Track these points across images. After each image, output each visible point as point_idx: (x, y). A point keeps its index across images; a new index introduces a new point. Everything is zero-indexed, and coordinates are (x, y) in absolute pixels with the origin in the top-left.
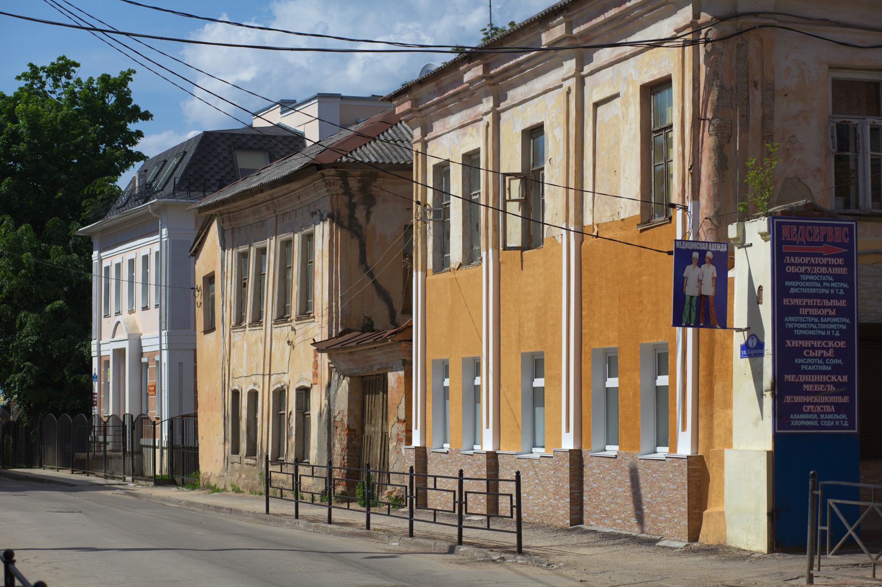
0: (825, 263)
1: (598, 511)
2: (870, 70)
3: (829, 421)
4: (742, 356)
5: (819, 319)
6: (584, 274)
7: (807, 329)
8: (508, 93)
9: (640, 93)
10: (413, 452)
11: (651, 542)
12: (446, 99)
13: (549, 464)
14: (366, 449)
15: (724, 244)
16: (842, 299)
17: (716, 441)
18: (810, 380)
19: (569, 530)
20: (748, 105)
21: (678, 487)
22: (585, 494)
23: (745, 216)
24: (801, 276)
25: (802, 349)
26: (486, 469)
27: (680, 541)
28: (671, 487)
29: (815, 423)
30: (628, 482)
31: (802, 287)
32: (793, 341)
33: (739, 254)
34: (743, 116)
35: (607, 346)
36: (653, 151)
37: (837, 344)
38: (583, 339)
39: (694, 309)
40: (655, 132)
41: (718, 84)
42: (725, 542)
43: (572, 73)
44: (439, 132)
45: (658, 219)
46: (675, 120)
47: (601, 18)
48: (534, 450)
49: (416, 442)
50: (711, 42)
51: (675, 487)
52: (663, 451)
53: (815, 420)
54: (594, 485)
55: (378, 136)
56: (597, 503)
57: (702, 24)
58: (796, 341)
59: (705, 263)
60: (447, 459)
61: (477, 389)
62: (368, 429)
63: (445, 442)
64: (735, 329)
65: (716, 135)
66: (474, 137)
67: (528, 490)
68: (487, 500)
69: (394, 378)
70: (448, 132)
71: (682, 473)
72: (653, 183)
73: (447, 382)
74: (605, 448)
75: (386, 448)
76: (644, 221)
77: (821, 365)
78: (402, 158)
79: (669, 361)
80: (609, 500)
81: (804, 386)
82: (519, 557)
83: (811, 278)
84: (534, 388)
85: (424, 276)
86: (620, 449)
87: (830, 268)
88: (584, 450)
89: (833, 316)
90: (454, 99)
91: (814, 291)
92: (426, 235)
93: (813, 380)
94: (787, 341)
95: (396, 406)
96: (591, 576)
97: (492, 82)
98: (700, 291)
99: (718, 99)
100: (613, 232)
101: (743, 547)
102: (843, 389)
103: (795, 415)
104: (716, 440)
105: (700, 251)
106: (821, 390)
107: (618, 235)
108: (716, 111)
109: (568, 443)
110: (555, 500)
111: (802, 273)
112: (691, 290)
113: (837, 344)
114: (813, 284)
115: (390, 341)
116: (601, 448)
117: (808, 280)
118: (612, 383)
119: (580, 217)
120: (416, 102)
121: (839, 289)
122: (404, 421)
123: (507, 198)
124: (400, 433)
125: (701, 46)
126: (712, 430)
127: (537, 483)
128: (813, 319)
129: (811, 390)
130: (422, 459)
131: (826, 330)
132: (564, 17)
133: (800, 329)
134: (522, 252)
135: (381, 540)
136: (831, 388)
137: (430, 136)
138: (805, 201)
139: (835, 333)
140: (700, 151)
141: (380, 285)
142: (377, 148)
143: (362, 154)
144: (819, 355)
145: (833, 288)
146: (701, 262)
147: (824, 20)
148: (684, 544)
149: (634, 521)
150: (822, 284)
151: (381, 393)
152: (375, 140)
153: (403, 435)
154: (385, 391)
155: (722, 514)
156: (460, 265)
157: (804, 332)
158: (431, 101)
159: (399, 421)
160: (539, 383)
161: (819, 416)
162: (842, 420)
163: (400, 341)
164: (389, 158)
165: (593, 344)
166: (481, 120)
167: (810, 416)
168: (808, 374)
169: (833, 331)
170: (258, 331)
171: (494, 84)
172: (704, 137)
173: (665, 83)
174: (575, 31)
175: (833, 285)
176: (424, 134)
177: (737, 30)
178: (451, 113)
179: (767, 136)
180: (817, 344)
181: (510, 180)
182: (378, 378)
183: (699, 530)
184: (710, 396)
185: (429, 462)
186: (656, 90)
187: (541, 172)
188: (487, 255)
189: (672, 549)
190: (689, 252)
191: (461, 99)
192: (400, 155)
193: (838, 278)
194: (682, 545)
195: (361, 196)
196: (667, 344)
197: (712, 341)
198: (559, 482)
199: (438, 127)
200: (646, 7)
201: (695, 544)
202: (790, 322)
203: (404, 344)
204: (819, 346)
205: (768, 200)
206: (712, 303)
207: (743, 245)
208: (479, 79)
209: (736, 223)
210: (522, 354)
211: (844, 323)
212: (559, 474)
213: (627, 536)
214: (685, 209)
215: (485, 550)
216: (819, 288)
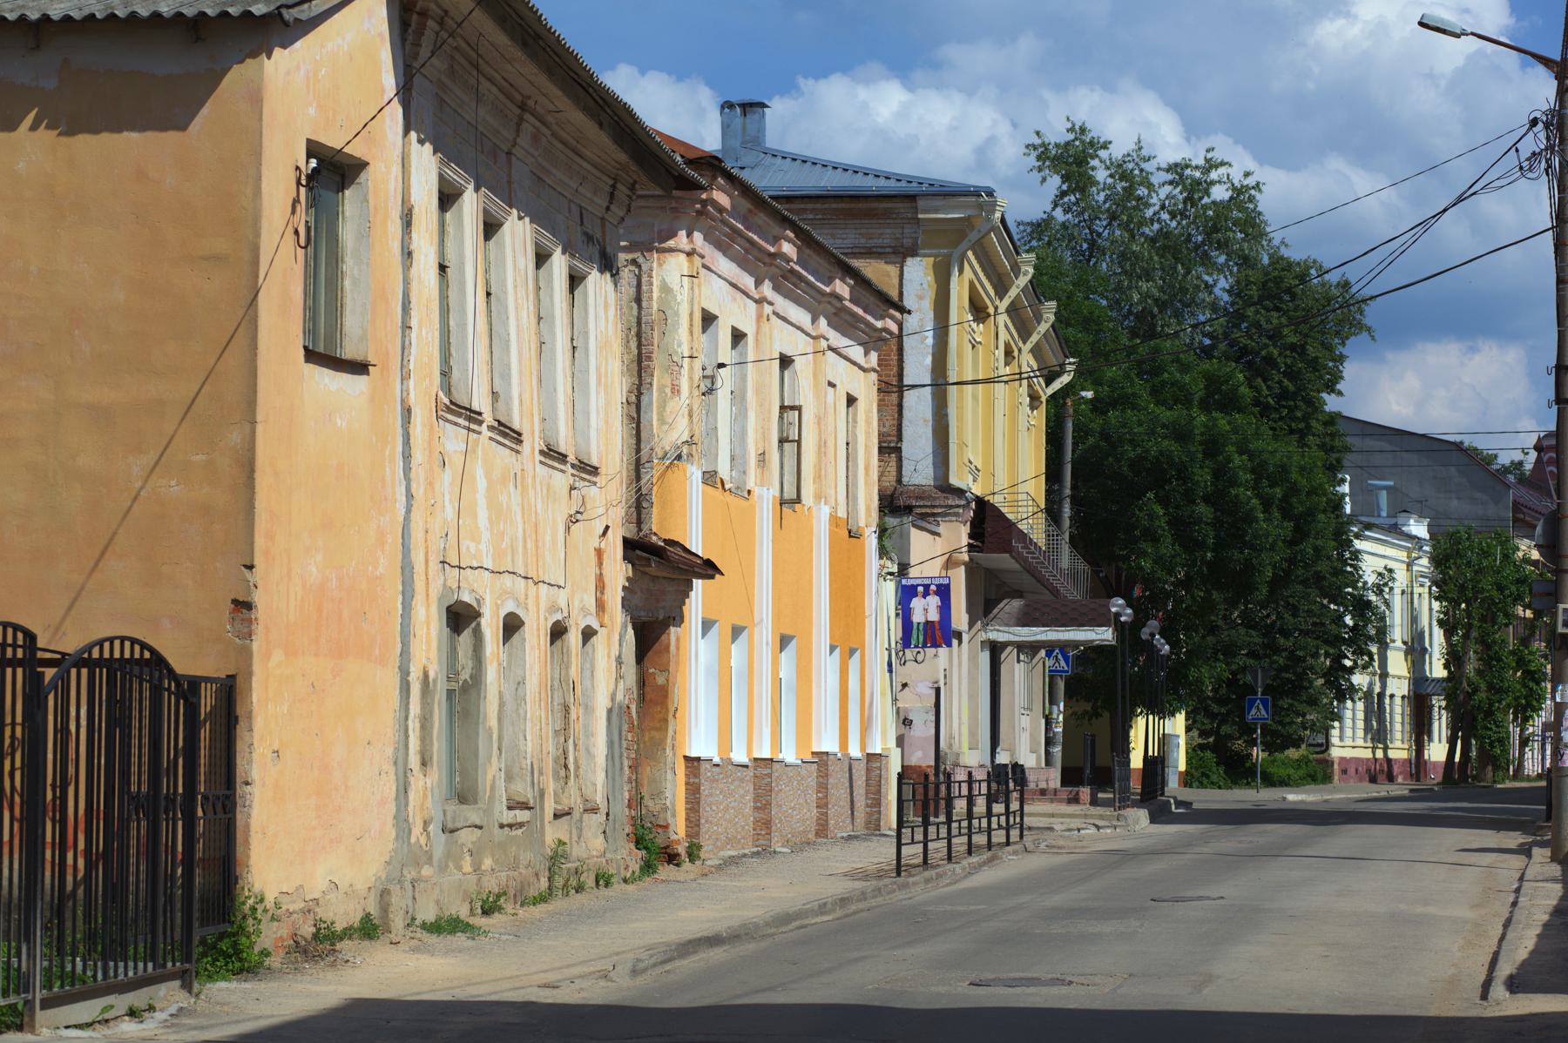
39: (921, 633)
105: (924, 586)
112: (918, 618)
146: (926, 594)
170: (507, 451)
206: (937, 627)
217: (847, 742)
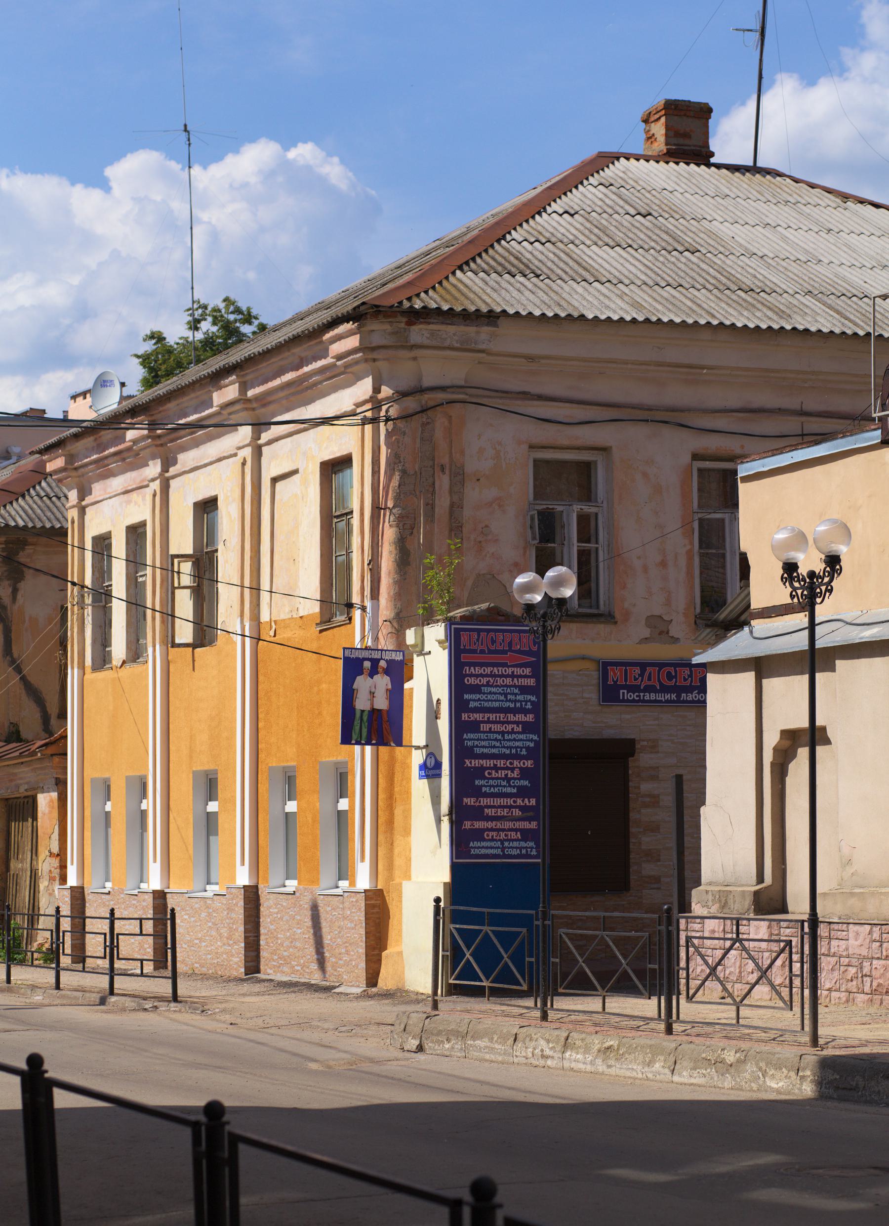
0: (510, 673)
1: (276, 957)
2: (578, 448)
3: (515, 850)
4: (421, 777)
5: (503, 736)
6: (261, 678)
7: (488, 747)
8: (178, 456)
9: (321, 471)
10: (67, 893)
11: (328, 989)
12: (106, 457)
13: (222, 904)
14: (12, 891)
15: (400, 651)
16: (529, 713)
17: (397, 873)
18: (492, 804)
19: (242, 980)
20: (433, 493)
21: (356, 925)
22: (262, 937)
23: (428, 619)
24: (483, 688)
25: (483, 769)
26: (152, 912)
27: (358, 986)
28: (349, 925)
29: (499, 852)
30: (308, 923)
31: (484, 700)
32: (473, 761)
33: (418, 661)
34: (427, 504)
35: (286, 764)
36: (334, 539)
37: (524, 764)
38: (260, 756)
40: (337, 517)
41: (400, 468)
42: (404, 986)
43: (248, 441)
44: (100, 496)
45: (340, 618)
46: (355, 506)
47: (277, 382)
48: (208, 887)
49: (72, 880)
50: (392, 420)
51: (353, 925)
52: (344, 884)
53: (498, 848)
54: (272, 927)
55: (28, 491)
56: (274, 948)
57: (383, 400)
58: (477, 761)
59: (377, 673)
60: (109, 901)
61: (144, 813)
62: (13, 864)
63: (107, 880)
64: (414, 746)
65: (398, 526)
66: (139, 506)
67: (200, 935)
68: (154, 949)
69: (45, 801)
70: (110, 498)
71: (360, 909)
72: (334, 576)
73: (108, 807)
74: (284, 883)
75: (37, 889)
76: (324, 620)
77: (504, 786)
78: (58, 520)
79: (349, 782)
80: (286, 943)
81: (486, 810)
82: (173, 1004)
83: (494, 690)
84: (208, 813)
85: (82, 673)
86: (299, 884)
87: (515, 679)
88: (261, 886)
89: (519, 733)
90: (115, 458)
91: (496, 704)
92: (84, 623)
93: (495, 804)
94: (467, 761)
95: (47, 837)
96: (245, 1021)
97: (159, 442)
98: (372, 704)
99: (399, 485)
100: (292, 631)
101: (421, 991)
102: (531, 814)
103: (475, 842)
104: (397, 872)
106: (505, 814)
107: (296, 635)
108: (397, 499)
109: (243, 878)
110: (229, 945)
111: (483, 685)
112: (362, 703)
113: (524, 764)
114: (495, 697)
115: (39, 755)
116: (280, 883)
117: (490, 693)
118: (291, 807)
119: (256, 612)
120: (71, 458)
121: (526, 702)
122: (58, 855)
123: (176, 585)
124: (53, 869)
125: (382, 424)
126: (392, 861)
127: (210, 927)
128: (496, 736)
129: (493, 814)
130: (79, 902)
131: (511, 748)
132: (237, 376)
133: (481, 747)
134: (193, 649)
135: (23, 995)
136: (517, 813)
137: (88, 500)
138: (488, 604)
139: (521, 751)
140: (380, 544)
141: (30, 682)
142: (27, 507)
143: (7, 515)
144: (503, 776)
145: (519, 701)
146: (373, 672)
147: (524, 393)
148: (362, 989)
149: (314, 966)
150: (506, 697)
151: (30, 820)
152: (23, 496)
153: (56, 873)
154: (35, 818)
155: (400, 954)
156: (124, 662)
157: (486, 751)
158: (88, 459)
159: (51, 854)
160: (213, 807)
161: (502, 844)
162: (530, 848)
163: (52, 755)
164: (42, 522)
165: (271, 761)
166: (147, 486)
167: (493, 844)
168: (490, 797)
169: (519, 750)
171: (162, 445)
172: (385, 528)
173: (345, 462)
174: (250, 393)
175: (518, 698)
176: (81, 498)
177: (422, 407)
178: (112, 474)
179: (455, 528)
180: (501, 763)
181: (179, 563)
182: (26, 800)
183: (377, 973)
184: (390, 822)
185: (87, 905)
186: (337, 469)
187: (215, 554)
188: (154, 652)
189: (347, 994)
190: (360, 661)
191: (124, 460)
192: (56, 517)
193: (524, 690)
194: (358, 990)
195: (5, 569)
196: (346, 763)
197: (392, 760)
198: (233, 924)
199: (98, 489)
200: (325, 373)
201: (374, 990)
202: (469, 740)
203: (56, 759)
204: (502, 765)
205: (448, 602)
206: (385, 716)
207: (421, 653)
208: (144, 438)
209: (413, 629)
210: (194, 772)
211: (532, 740)
212: (233, 915)
213: (304, 984)
214: (363, 609)
215: (136, 999)
216: (502, 701)
217: (176, 979)
